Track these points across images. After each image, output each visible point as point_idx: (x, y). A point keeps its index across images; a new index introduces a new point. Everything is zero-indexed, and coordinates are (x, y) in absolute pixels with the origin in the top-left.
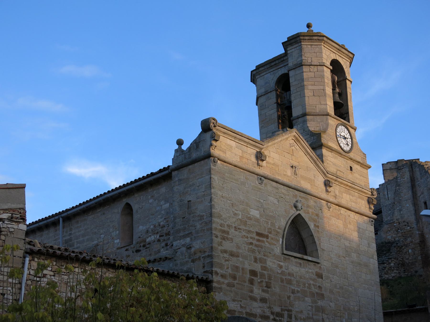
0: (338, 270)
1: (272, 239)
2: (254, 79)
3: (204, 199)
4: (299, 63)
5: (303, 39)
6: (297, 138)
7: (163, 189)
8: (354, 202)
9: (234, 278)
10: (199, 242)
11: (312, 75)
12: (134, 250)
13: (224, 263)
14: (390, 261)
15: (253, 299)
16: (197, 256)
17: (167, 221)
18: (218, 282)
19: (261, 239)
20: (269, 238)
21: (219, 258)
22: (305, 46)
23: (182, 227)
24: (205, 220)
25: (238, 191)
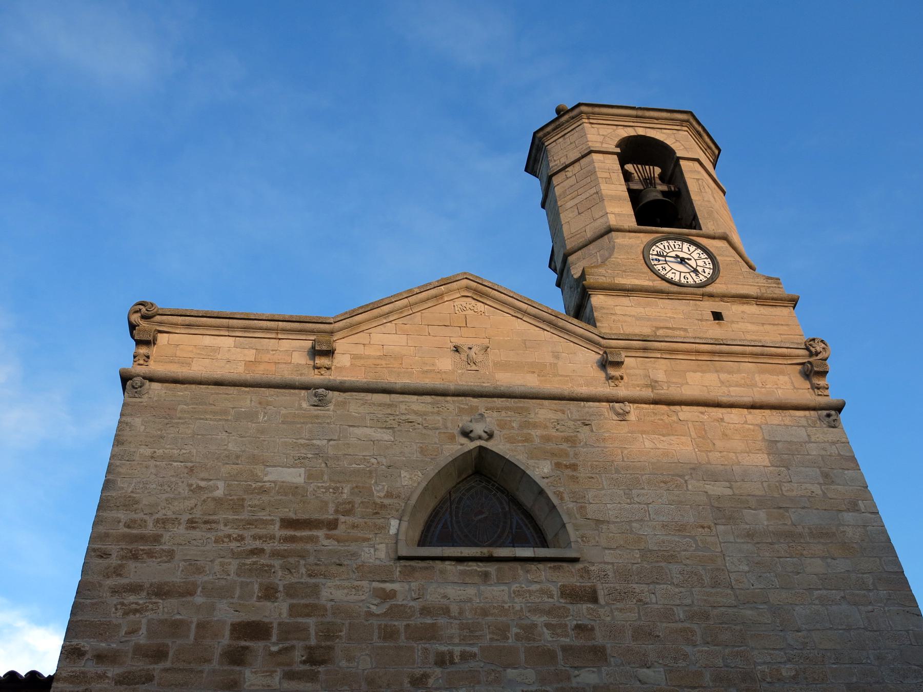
5: (545, 135)
6: (476, 291)
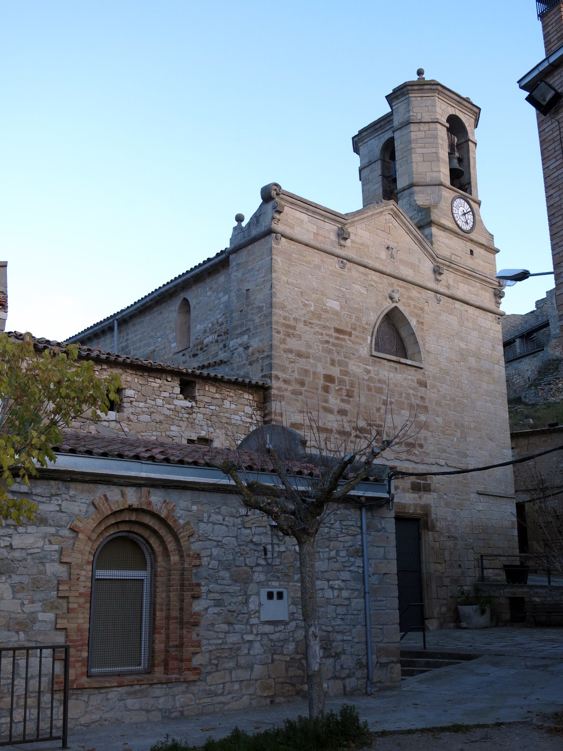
0: (448, 377)
1: (357, 337)
2: (356, 148)
3: (264, 286)
4: (405, 120)
5: (412, 90)
6: (395, 212)
7: (221, 278)
8: (474, 294)
9: (302, 384)
10: (257, 339)
11: (421, 134)
12: (191, 354)
13: (287, 366)
14: (557, 381)
15: (329, 410)
16: (254, 358)
17: (226, 317)
18: (279, 389)
19: (341, 336)
20: (353, 336)
21: (280, 358)
22: (414, 99)
23: (240, 322)
24: (264, 312)
25: (310, 276)
